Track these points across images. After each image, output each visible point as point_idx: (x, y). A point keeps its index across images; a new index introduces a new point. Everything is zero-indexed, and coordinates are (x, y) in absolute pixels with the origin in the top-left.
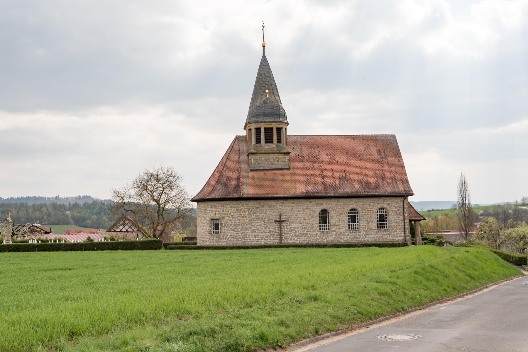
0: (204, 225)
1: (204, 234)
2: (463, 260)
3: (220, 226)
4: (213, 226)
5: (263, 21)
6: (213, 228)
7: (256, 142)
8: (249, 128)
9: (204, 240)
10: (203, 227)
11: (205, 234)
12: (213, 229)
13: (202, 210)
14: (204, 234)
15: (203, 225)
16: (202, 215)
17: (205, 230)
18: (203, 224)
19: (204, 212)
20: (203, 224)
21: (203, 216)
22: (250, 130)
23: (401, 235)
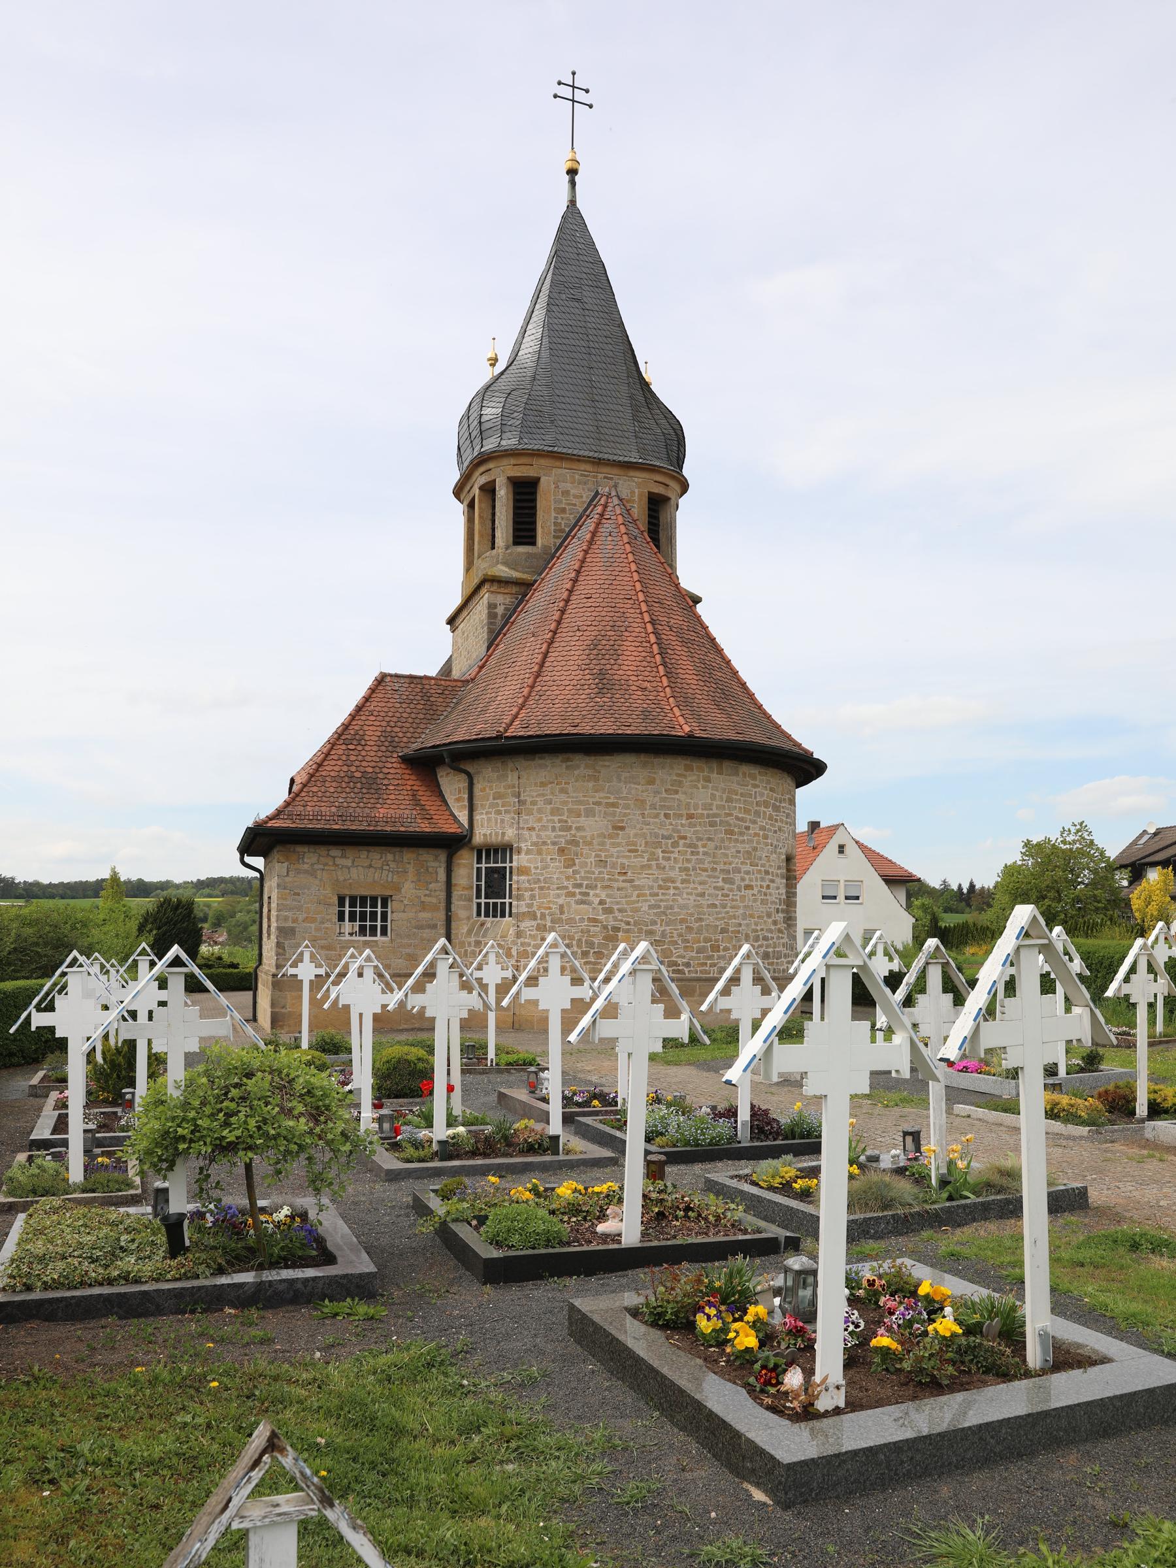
0: (772, 881)
1: (770, 920)
2: (96, 975)
3: (510, 880)
4: (479, 879)
5: (574, 73)
6: (479, 888)
7: (515, 537)
8: (482, 480)
9: (770, 950)
10: (768, 887)
11: (775, 923)
12: (478, 896)
13: (758, 804)
14: (770, 920)
15: (763, 879)
16: (763, 828)
17: (773, 902)
18: (767, 873)
19: (771, 818)
20: (767, 873)
21: (766, 837)
22: (489, 490)
23: (654, 928)
